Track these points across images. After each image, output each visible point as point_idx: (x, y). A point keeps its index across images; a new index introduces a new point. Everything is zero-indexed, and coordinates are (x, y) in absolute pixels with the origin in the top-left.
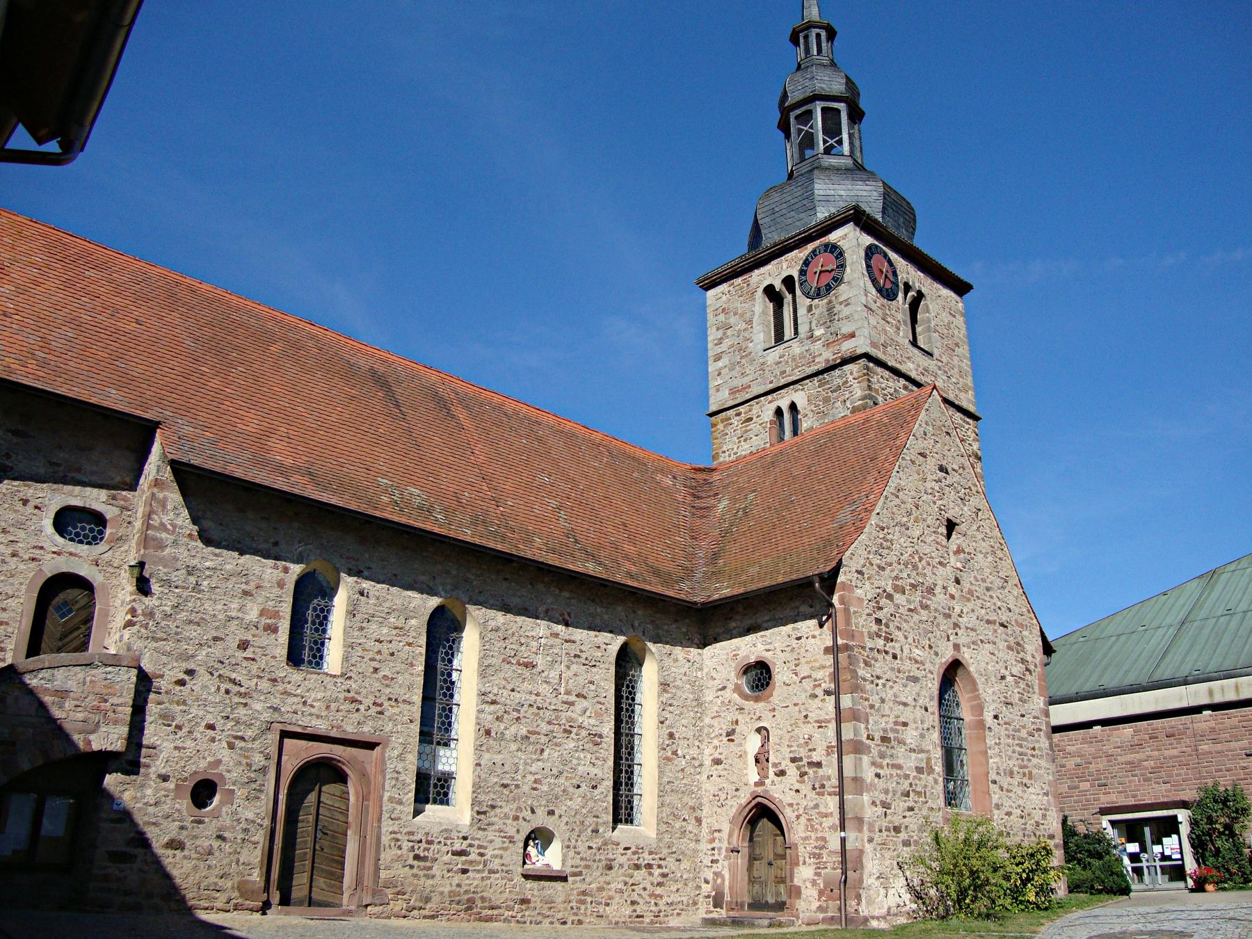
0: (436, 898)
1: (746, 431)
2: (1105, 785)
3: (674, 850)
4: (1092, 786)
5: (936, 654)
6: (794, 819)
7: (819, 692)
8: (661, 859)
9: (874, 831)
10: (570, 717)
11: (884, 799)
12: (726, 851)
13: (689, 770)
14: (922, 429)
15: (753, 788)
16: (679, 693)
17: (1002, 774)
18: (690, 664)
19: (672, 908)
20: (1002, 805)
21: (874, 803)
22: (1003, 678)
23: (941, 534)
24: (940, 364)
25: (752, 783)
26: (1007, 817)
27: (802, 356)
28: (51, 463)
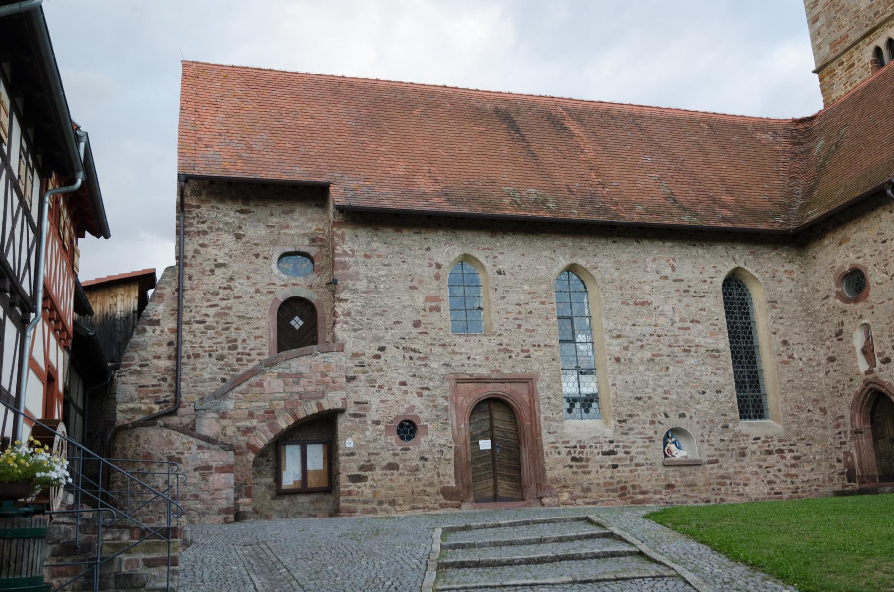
0: (594, 488)
1: (851, 76)
3: (803, 436)
8: (791, 445)
10: (687, 339)
18: (795, 282)
19: (808, 484)
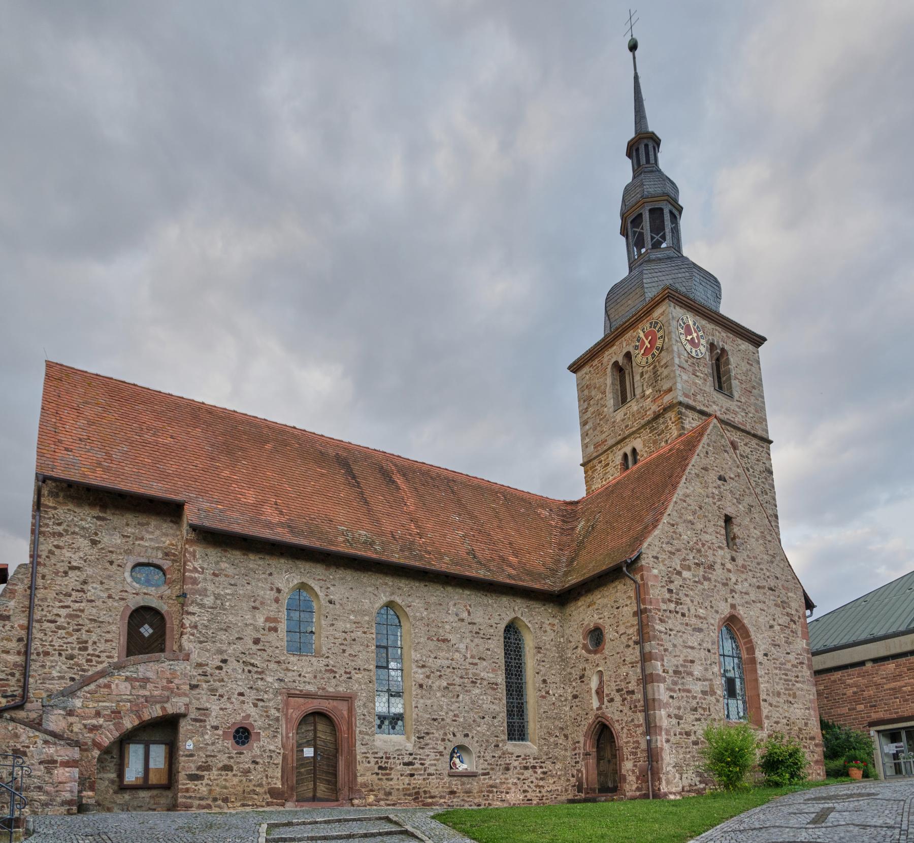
0: (394, 792)
1: (606, 473)
2: (875, 706)
4: (866, 707)
7: (631, 643)
8: (541, 762)
14: (705, 450)
15: (596, 712)
16: (548, 653)
21: (669, 716)
22: (771, 627)
25: (595, 708)
27: (638, 412)
28: (124, 536)
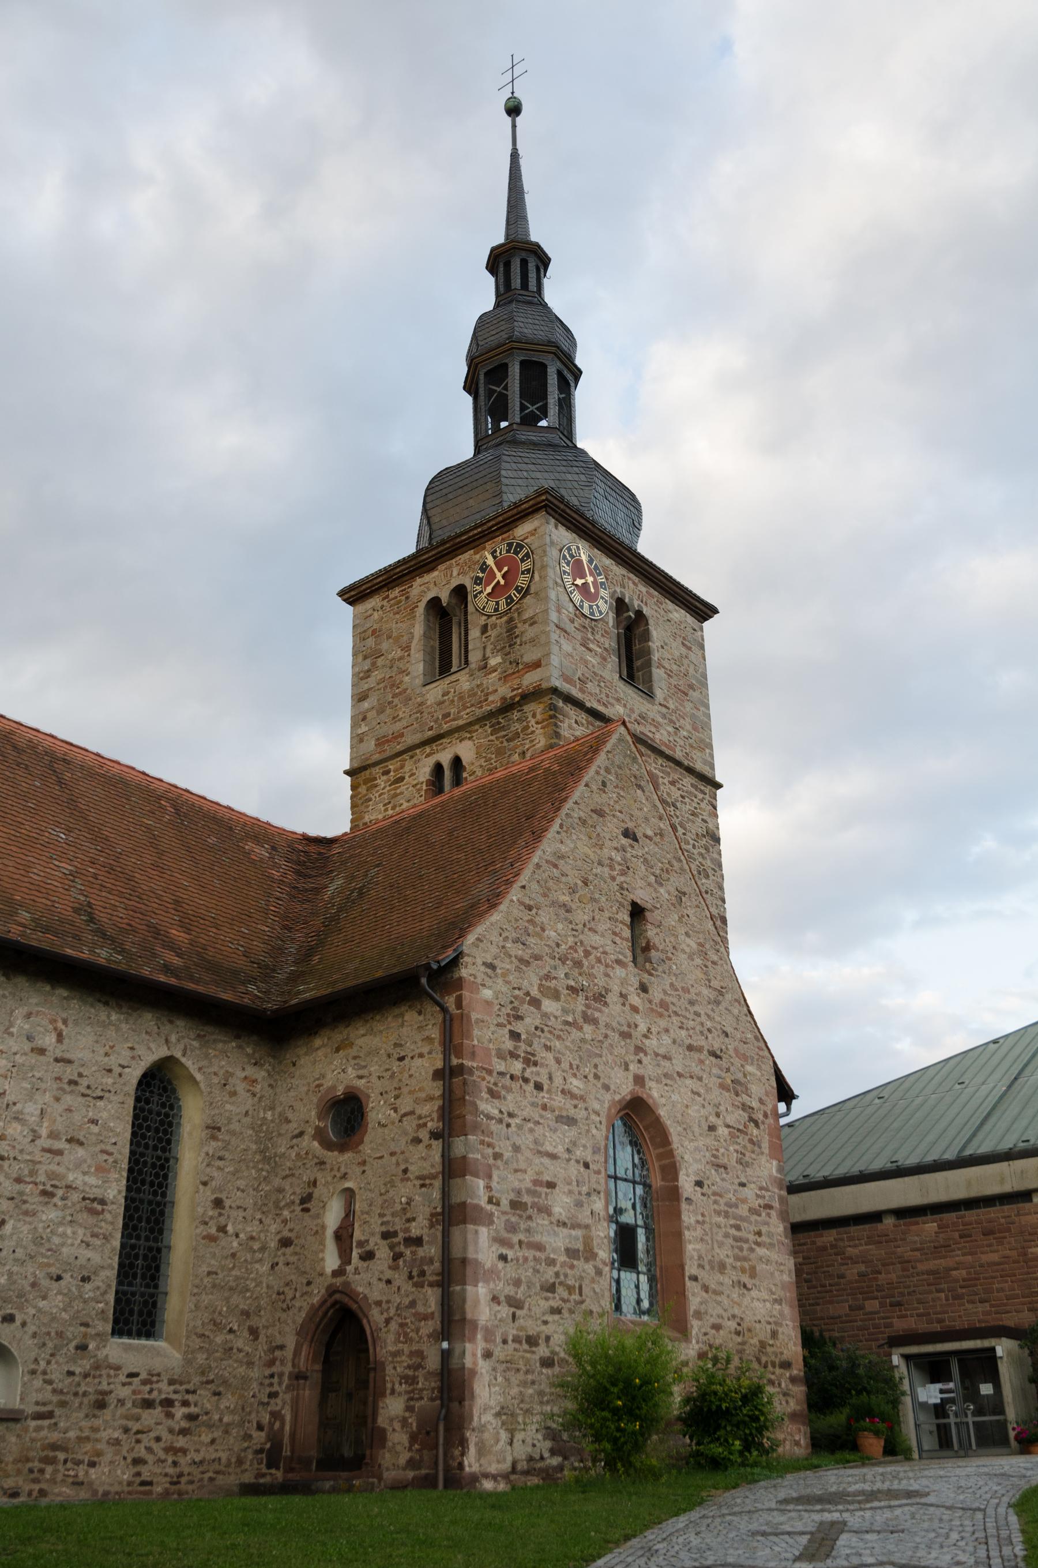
1: (396, 795)
2: (899, 1304)
3: (211, 1377)
4: (883, 1305)
5: (606, 1088)
6: (382, 1325)
7: (424, 1135)
8: (188, 1392)
9: (494, 1341)
11: (512, 1293)
12: (290, 1378)
13: (244, 1256)
14: (600, 778)
15: (330, 1280)
17: (707, 1267)
19: (201, 1469)
20: (706, 1313)
21: (495, 1299)
22: (712, 1128)
23: (621, 922)
24: (664, 710)
26: (714, 1331)
27: (472, 693)
